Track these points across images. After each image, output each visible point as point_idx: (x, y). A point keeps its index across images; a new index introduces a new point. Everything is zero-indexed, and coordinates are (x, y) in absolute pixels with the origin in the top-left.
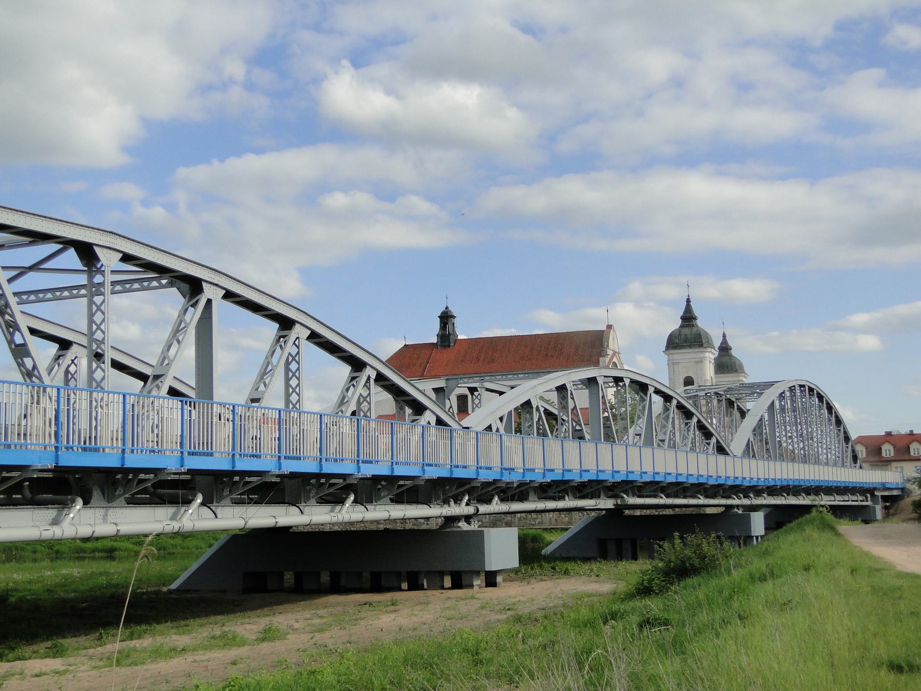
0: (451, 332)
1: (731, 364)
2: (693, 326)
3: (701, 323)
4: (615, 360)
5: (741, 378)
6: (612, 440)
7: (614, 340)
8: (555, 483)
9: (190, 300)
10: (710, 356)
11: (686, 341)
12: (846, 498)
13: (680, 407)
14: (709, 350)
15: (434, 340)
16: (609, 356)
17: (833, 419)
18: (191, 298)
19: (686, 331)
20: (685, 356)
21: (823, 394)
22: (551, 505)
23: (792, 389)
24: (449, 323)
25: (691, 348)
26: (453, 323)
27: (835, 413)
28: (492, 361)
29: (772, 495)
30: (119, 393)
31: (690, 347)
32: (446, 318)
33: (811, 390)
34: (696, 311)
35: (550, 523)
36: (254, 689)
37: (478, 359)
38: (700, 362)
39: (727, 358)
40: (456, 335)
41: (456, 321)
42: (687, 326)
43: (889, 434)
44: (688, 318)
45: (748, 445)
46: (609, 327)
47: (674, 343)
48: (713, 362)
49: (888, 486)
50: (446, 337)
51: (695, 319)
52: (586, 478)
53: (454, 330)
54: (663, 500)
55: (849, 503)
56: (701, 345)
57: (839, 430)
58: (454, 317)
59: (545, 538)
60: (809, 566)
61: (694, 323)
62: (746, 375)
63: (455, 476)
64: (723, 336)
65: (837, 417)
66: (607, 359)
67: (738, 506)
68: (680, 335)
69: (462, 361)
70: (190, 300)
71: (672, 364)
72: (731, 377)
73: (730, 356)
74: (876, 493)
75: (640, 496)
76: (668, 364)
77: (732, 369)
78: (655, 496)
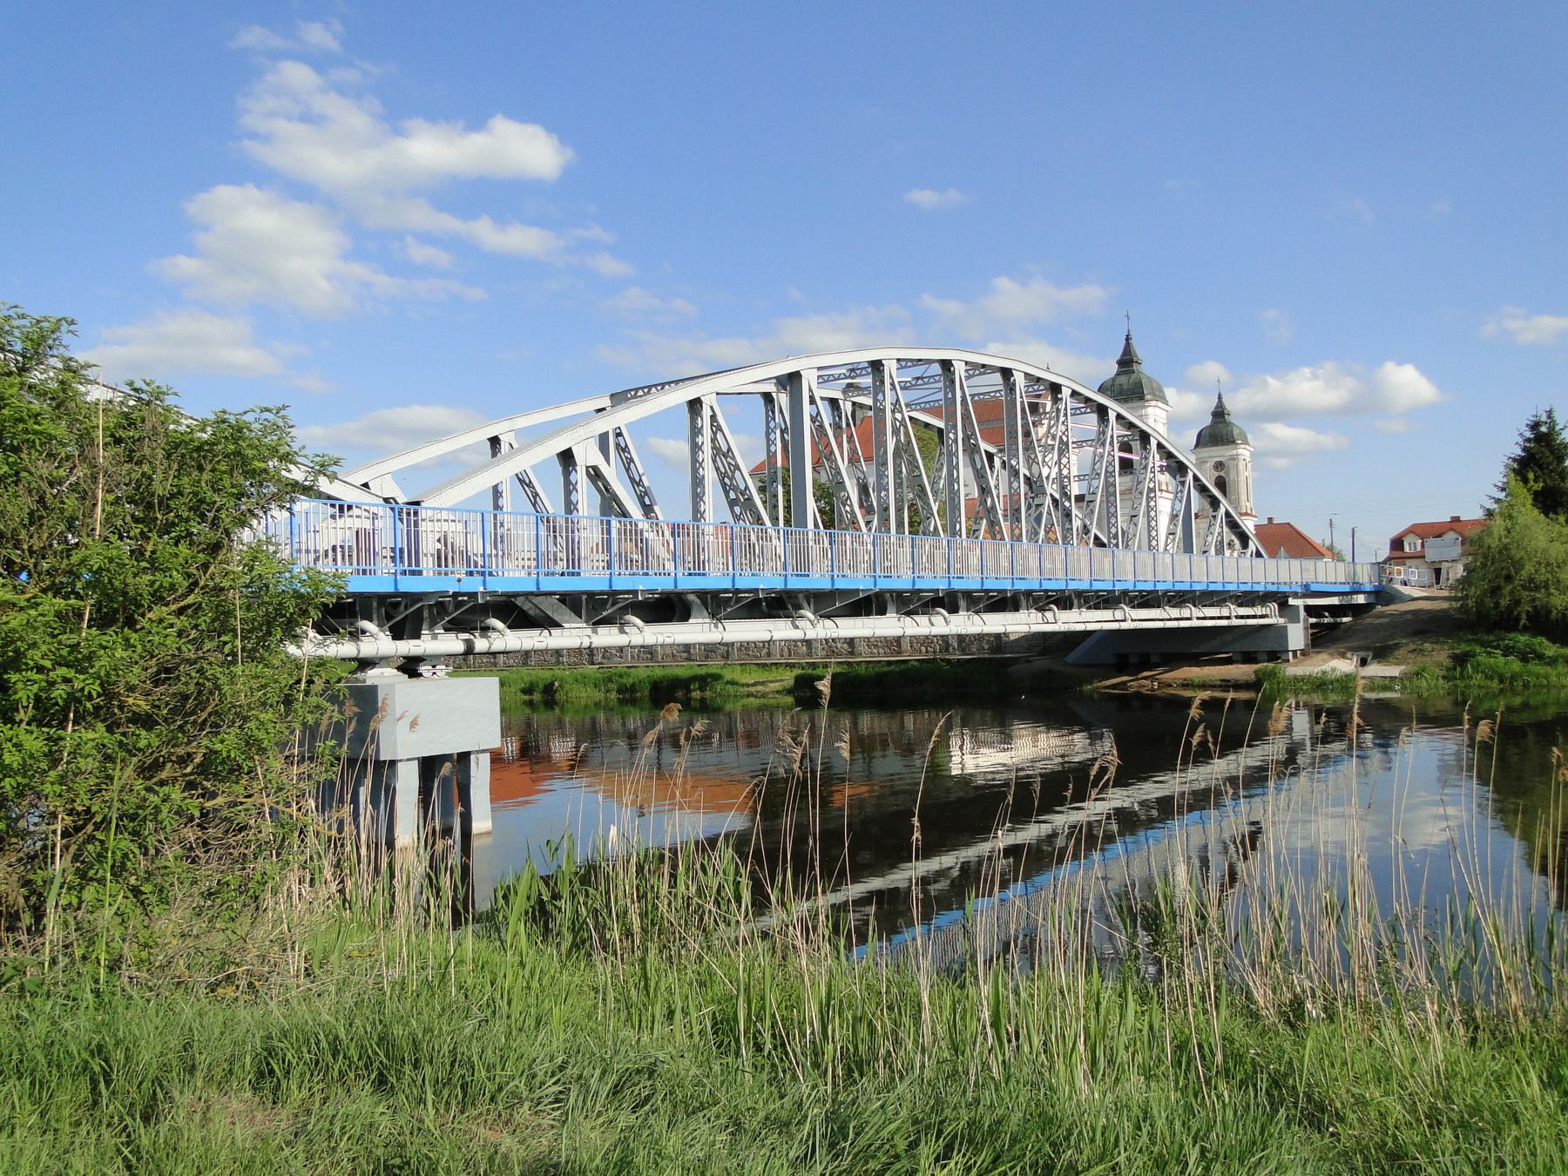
6: (998, 537)
12: (1186, 613)
14: (1154, 403)
19: (1123, 379)
30: (476, 512)
34: (1139, 350)
42: (1126, 373)
43: (1456, 520)
44: (1219, 414)
49: (1314, 588)
55: (1195, 623)
56: (1141, 397)
63: (402, 589)
64: (1121, 363)
73: (1228, 424)
74: (1291, 601)
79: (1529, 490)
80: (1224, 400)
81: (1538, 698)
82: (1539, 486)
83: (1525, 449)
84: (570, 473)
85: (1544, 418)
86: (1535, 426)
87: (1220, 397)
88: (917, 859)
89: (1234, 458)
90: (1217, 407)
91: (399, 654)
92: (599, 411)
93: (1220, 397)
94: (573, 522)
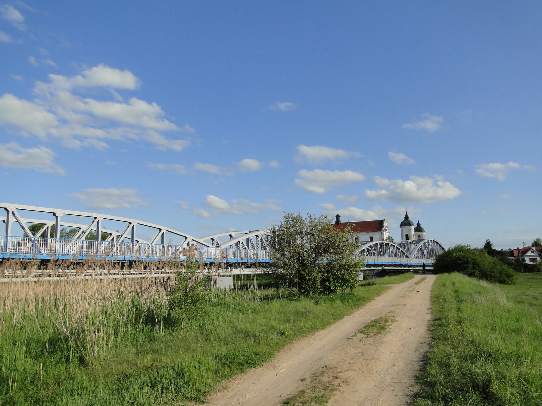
2: (408, 220)
3: (410, 218)
4: (386, 228)
8: (377, 264)
13: (397, 248)
14: (413, 226)
17: (441, 248)
19: (406, 221)
20: (406, 228)
22: (369, 269)
23: (428, 241)
33: (434, 241)
35: (368, 274)
38: (410, 230)
41: (340, 218)
42: (407, 220)
44: (407, 217)
47: (403, 224)
50: (338, 222)
51: (409, 218)
52: (375, 263)
54: (392, 268)
56: (410, 225)
58: (340, 217)
60: (510, 313)
64: (405, 218)
66: (384, 228)
67: (412, 270)
68: (404, 222)
71: (402, 230)
75: (388, 267)
78: (391, 267)
80: (419, 222)
82: (488, 251)
83: (486, 245)
84: (211, 266)
86: (487, 241)
87: (418, 221)
88: (239, 275)
89: (422, 235)
90: (418, 223)
92: (245, 234)
93: (418, 221)
94: (207, 353)
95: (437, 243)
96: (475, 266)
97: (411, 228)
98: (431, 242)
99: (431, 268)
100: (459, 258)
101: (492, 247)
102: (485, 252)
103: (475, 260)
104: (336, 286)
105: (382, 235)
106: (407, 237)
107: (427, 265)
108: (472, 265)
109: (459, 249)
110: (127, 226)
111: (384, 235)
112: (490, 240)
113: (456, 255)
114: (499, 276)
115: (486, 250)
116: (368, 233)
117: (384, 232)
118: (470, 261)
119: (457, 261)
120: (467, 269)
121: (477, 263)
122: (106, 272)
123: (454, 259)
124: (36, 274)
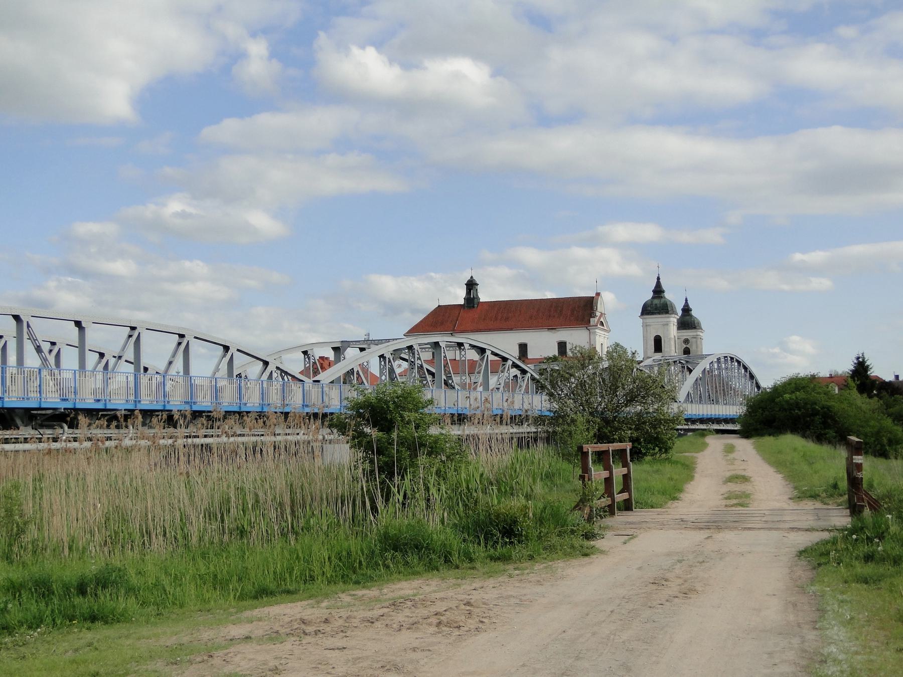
0: (475, 296)
1: (691, 322)
3: (669, 295)
4: (602, 320)
5: (699, 333)
7: (601, 304)
9: (481, 356)
10: (673, 320)
11: (656, 309)
14: (673, 315)
15: (462, 302)
16: (598, 317)
17: (748, 374)
18: (482, 355)
19: (656, 301)
20: (656, 321)
21: (740, 360)
24: (474, 289)
25: (659, 314)
26: (477, 290)
27: (749, 371)
28: (507, 319)
29: (702, 424)
30: (72, 370)
31: (659, 313)
32: (471, 285)
33: (732, 358)
34: (664, 286)
36: (62, 676)
37: (496, 319)
38: (667, 324)
39: (688, 317)
40: (478, 298)
44: (658, 291)
45: (688, 395)
46: (598, 294)
47: (647, 310)
48: (676, 324)
50: (471, 301)
53: (477, 295)
56: (667, 312)
57: (753, 382)
59: (801, 376)
61: (662, 295)
62: (703, 331)
64: (655, 292)
65: (750, 373)
66: (596, 319)
68: (652, 304)
69: (484, 319)
70: (481, 356)
71: (645, 326)
72: (691, 332)
73: (691, 316)
76: (642, 326)
77: (692, 326)
79: (856, 384)
81: (778, 399)
83: (854, 367)
85: (861, 356)
86: (858, 358)
87: (686, 300)
90: (684, 306)
91: (30, 444)
93: (686, 300)
95: (739, 362)
96: (829, 421)
97: (668, 320)
98: (726, 361)
99: (737, 427)
100: (797, 405)
101: (869, 373)
102: (852, 384)
103: (828, 408)
104: (648, 449)
105: (592, 337)
106: (658, 344)
107: (715, 419)
108: (821, 419)
109: (796, 384)
110: (126, 336)
111: (597, 338)
112: (864, 355)
113: (790, 399)
114: (875, 441)
115: (854, 381)
116: (553, 331)
117: (597, 331)
118: (819, 411)
119: (793, 412)
120: (812, 428)
121: (833, 414)
122: (246, 431)
123: (786, 407)
124: (69, 435)
